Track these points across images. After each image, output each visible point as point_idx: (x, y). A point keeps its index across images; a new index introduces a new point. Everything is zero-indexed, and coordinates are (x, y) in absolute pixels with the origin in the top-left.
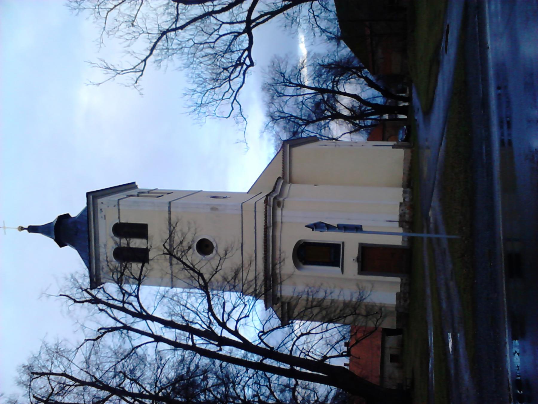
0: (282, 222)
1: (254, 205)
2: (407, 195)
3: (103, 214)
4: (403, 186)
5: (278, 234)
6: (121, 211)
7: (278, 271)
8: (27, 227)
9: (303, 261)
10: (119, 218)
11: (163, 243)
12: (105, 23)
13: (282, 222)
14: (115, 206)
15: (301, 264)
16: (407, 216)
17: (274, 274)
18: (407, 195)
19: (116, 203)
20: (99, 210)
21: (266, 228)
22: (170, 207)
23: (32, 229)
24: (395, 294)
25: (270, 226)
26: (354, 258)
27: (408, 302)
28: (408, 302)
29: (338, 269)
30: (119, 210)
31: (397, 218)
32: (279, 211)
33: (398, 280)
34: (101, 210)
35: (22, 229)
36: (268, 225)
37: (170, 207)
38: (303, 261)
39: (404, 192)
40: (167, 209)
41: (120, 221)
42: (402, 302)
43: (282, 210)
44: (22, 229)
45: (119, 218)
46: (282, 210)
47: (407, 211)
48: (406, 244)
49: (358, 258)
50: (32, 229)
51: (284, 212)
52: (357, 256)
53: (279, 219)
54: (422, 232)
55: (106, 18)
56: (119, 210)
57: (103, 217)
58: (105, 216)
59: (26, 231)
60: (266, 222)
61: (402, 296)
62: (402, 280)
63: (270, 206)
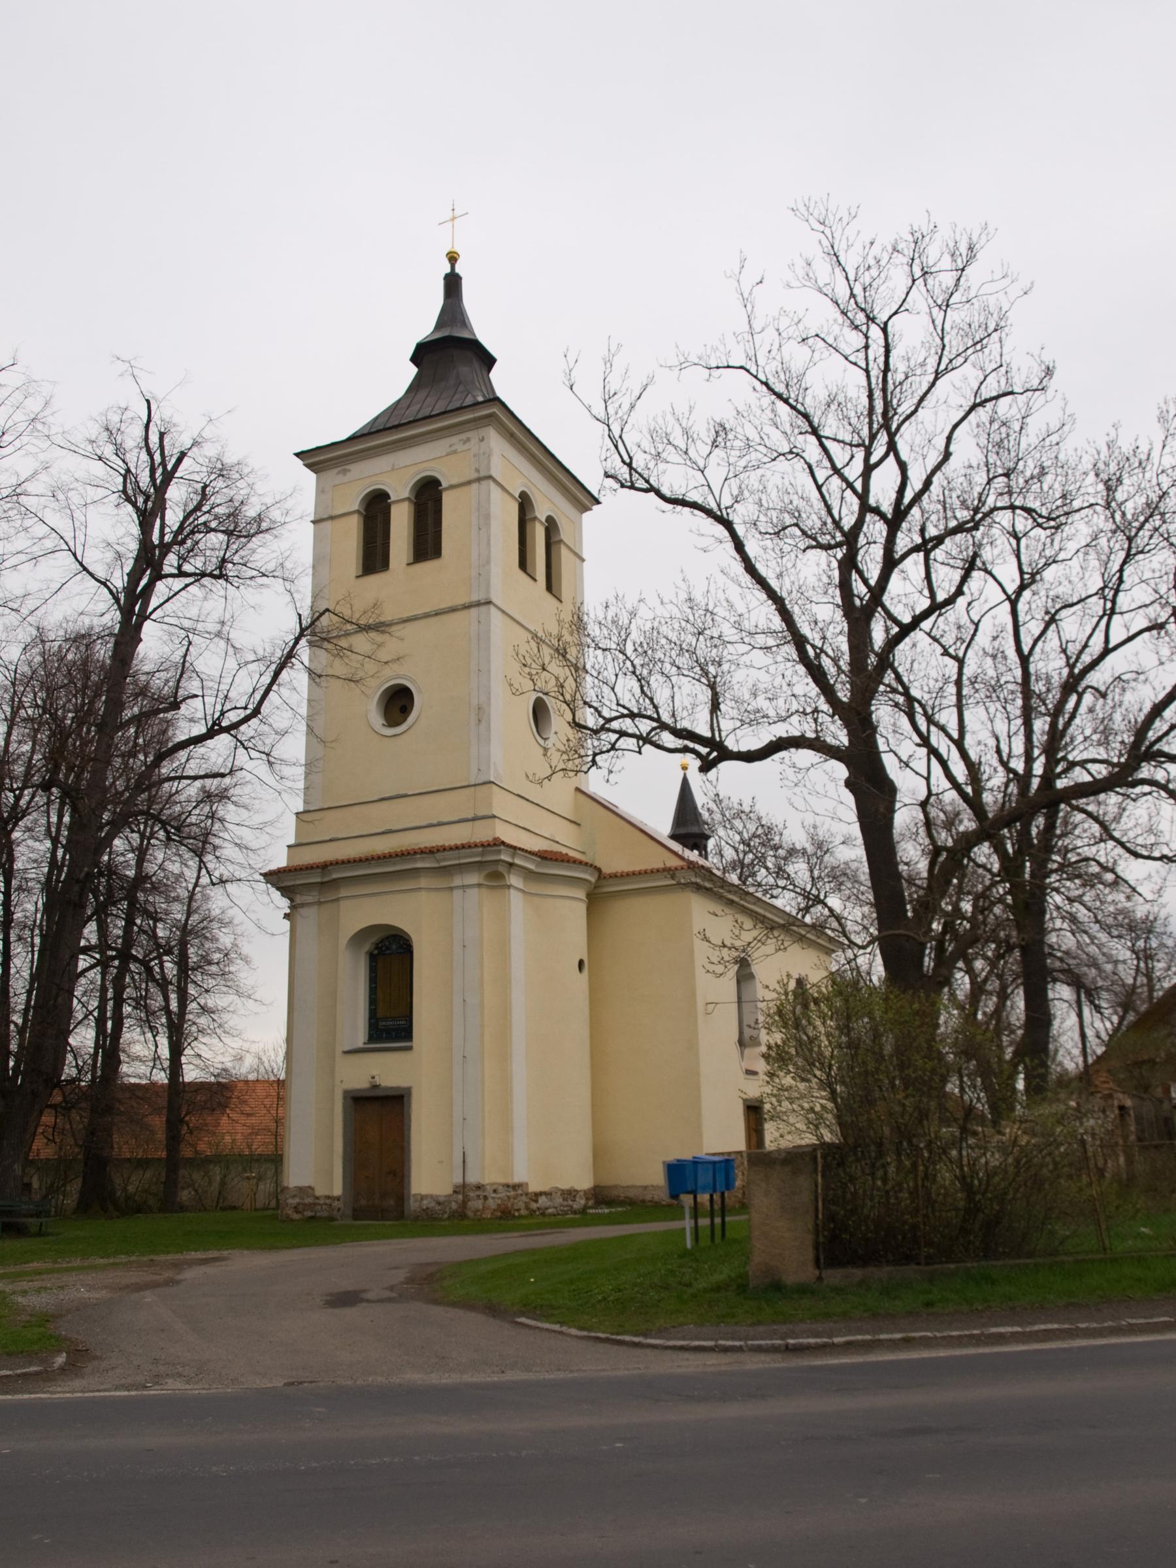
0: (451, 889)
1: (489, 814)
2: (559, 1200)
3: (460, 447)
4: (595, 1188)
5: (424, 882)
6: (465, 489)
7: (343, 893)
8: (458, 270)
9: (376, 952)
10: (452, 487)
11: (331, 608)
12: (718, 368)
13: (451, 889)
14: (478, 471)
15: (367, 947)
16: (478, 1204)
17: (335, 884)
18: (559, 1200)
19: (483, 474)
20: (468, 434)
21: (431, 852)
22: (478, 604)
23: (453, 284)
24: (313, 1185)
25: (438, 861)
26: (377, 1079)
27: (296, 1216)
28: (296, 1216)
29: (360, 1037)
30: (469, 483)
31: (472, 1179)
32: (473, 878)
33: (338, 1191)
34: (468, 440)
35: (453, 258)
36: (438, 856)
37: (478, 604)
38: (376, 952)
39: (570, 1194)
40: (475, 598)
41: (446, 489)
42: (293, 1202)
43: (479, 885)
44: (453, 258)
45: (452, 487)
46: (479, 885)
47: (492, 1204)
48: (413, 1205)
49: (375, 1087)
50: (453, 284)
51: (474, 892)
52: (383, 1084)
53: (457, 881)
54: (684, 1229)
55: (728, 367)
56: (469, 483)
57: (453, 448)
58: (455, 452)
59: (448, 270)
60: (444, 849)
61: (308, 1200)
62: (338, 1199)
63: (483, 854)
